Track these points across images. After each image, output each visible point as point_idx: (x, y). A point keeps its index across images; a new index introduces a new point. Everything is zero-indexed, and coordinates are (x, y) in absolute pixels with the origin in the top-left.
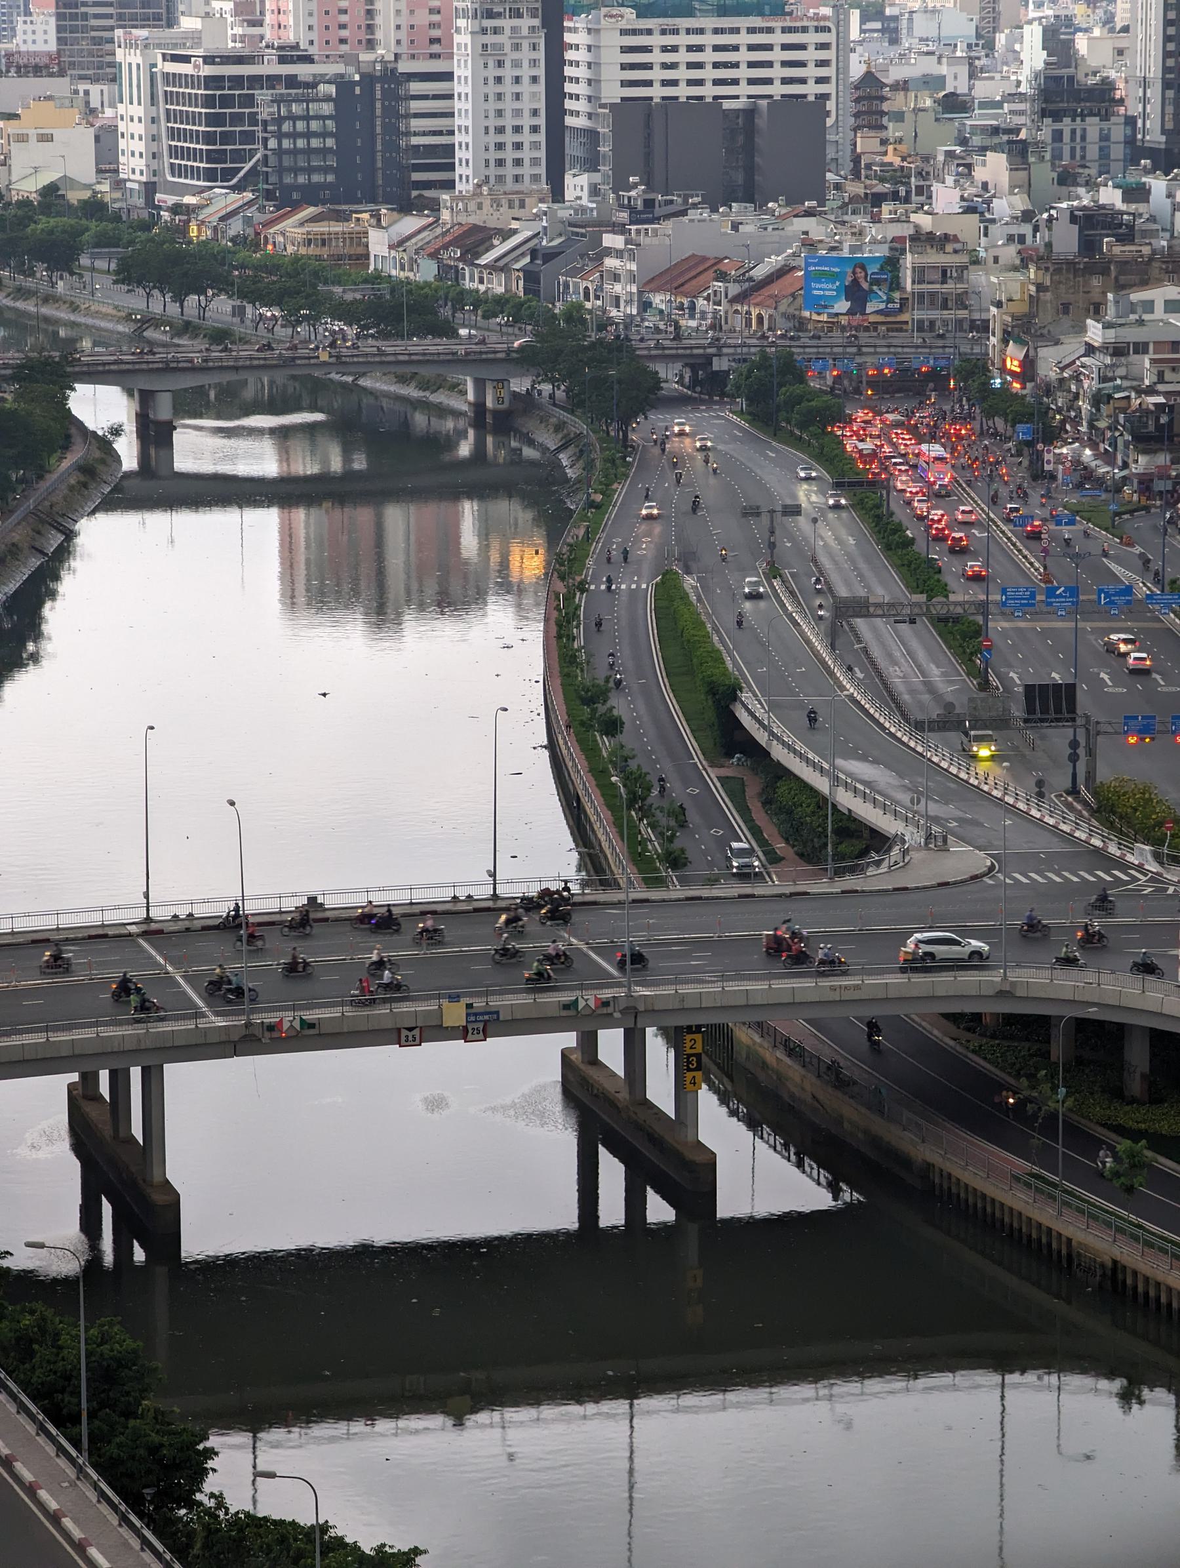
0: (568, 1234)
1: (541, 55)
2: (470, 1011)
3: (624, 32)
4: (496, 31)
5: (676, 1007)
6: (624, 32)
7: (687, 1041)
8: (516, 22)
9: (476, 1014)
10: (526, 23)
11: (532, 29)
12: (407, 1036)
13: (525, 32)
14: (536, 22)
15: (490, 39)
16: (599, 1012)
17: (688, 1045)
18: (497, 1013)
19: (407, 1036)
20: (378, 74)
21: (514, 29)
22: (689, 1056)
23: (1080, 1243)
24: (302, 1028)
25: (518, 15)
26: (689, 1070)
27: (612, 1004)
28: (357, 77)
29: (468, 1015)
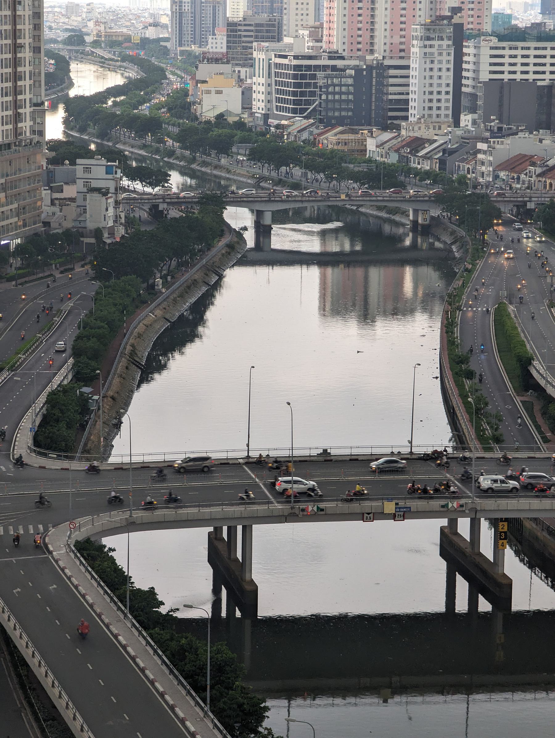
0: (440, 614)
1: (452, 58)
3: (492, 48)
4: (431, 46)
6: (492, 48)
7: (500, 525)
8: (441, 42)
9: (400, 508)
11: (448, 46)
13: (445, 47)
14: (450, 43)
15: (428, 50)
20: (375, 66)
24: (317, 511)
28: (365, 67)
29: (396, 508)
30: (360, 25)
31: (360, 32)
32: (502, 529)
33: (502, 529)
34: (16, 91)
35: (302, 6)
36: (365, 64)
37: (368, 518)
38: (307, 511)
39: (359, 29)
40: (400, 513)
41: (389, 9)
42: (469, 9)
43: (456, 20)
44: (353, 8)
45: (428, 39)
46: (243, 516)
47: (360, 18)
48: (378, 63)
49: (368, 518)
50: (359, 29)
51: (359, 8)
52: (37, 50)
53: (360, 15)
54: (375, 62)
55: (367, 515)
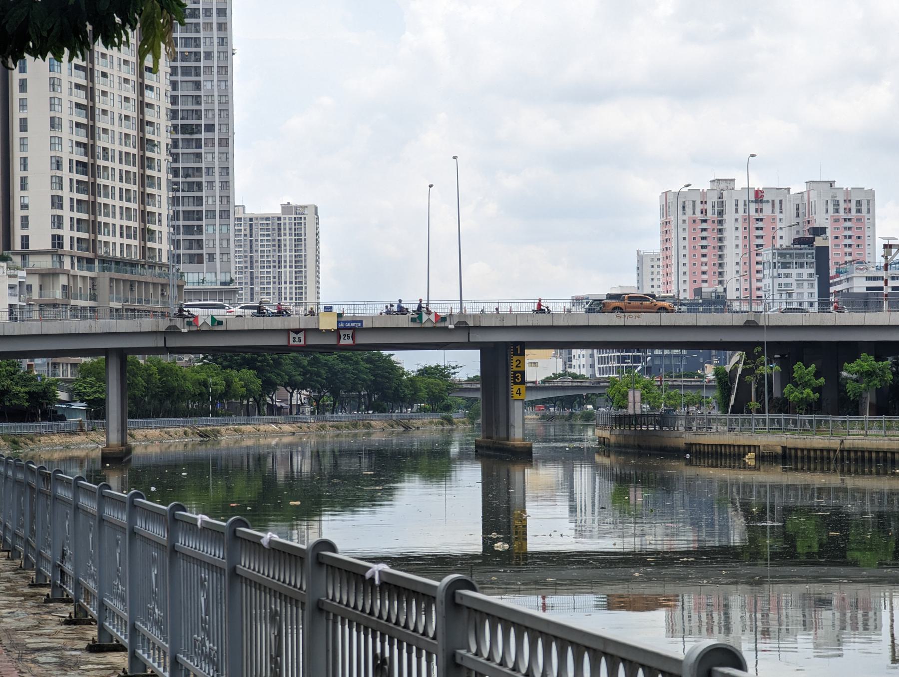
0: (474, 557)
1: (815, 290)
2: (340, 320)
3: (868, 278)
4: (787, 276)
5: (498, 324)
6: (868, 278)
7: (514, 361)
8: (800, 270)
9: (345, 322)
10: (806, 271)
11: (811, 275)
12: (294, 338)
13: (805, 277)
14: (813, 271)
15: (783, 280)
16: (438, 325)
17: (515, 364)
18: (361, 322)
19: (294, 338)
20: (713, 299)
21: (800, 275)
22: (515, 372)
23: (764, 446)
24: (213, 325)
25: (802, 266)
26: (515, 383)
27: (448, 319)
28: (701, 301)
29: (338, 322)
30: (704, 268)
31: (705, 277)
32: (517, 366)
33: (517, 366)
34: (145, 198)
35: (655, 280)
36: (701, 298)
37: (297, 340)
38: (197, 326)
39: (704, 273)
40: (346, 332)
41: (740, 246)
42: (846, 245)
43: (819, 242)
44: (694, 247)
45: (785, 265)
46: (93, 331)
47: (704, 259)
48: (718, 297)
49: (297, 340)
50: (704, 273)
51: (703, 247)
52: (225, 214)
53: (704, 256)
54: (713, 295)
55: (295, 335)
